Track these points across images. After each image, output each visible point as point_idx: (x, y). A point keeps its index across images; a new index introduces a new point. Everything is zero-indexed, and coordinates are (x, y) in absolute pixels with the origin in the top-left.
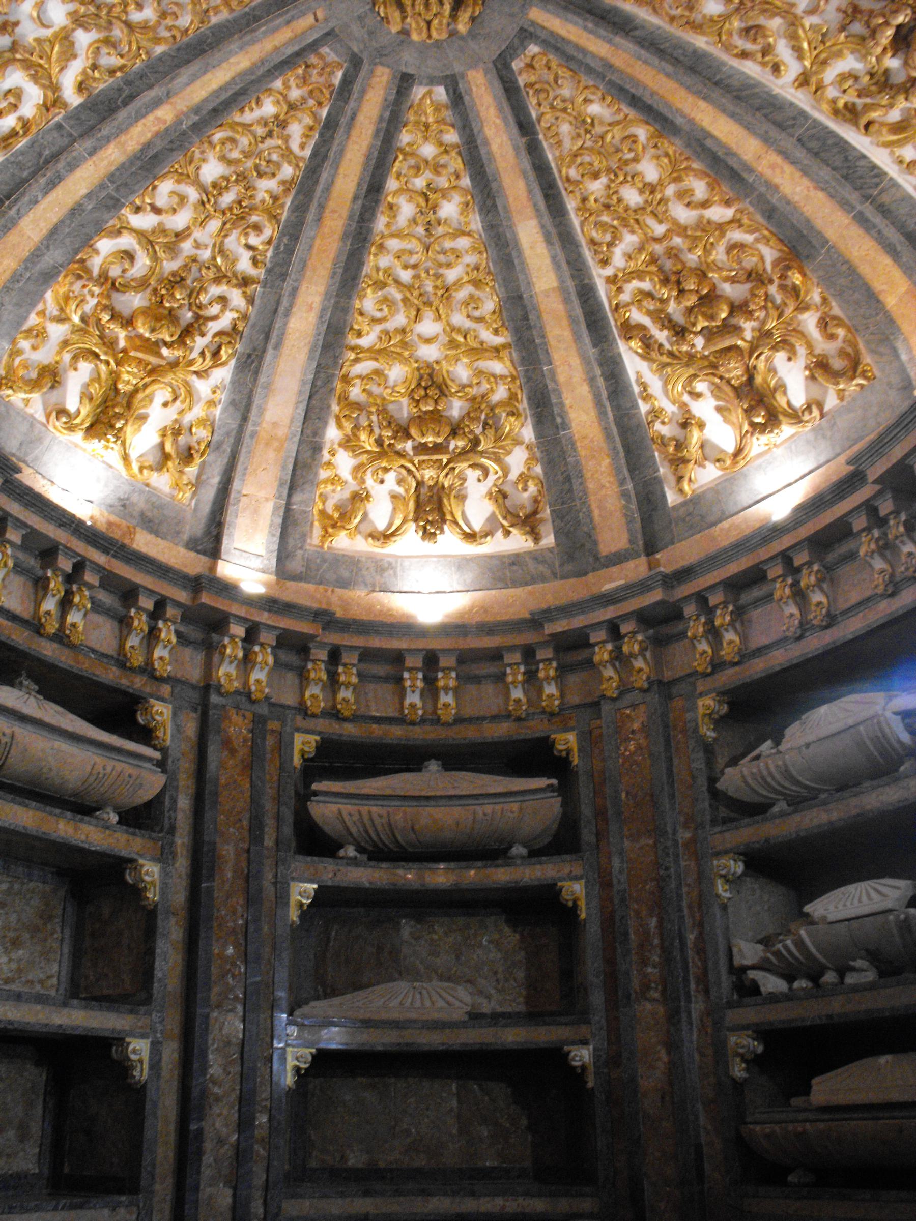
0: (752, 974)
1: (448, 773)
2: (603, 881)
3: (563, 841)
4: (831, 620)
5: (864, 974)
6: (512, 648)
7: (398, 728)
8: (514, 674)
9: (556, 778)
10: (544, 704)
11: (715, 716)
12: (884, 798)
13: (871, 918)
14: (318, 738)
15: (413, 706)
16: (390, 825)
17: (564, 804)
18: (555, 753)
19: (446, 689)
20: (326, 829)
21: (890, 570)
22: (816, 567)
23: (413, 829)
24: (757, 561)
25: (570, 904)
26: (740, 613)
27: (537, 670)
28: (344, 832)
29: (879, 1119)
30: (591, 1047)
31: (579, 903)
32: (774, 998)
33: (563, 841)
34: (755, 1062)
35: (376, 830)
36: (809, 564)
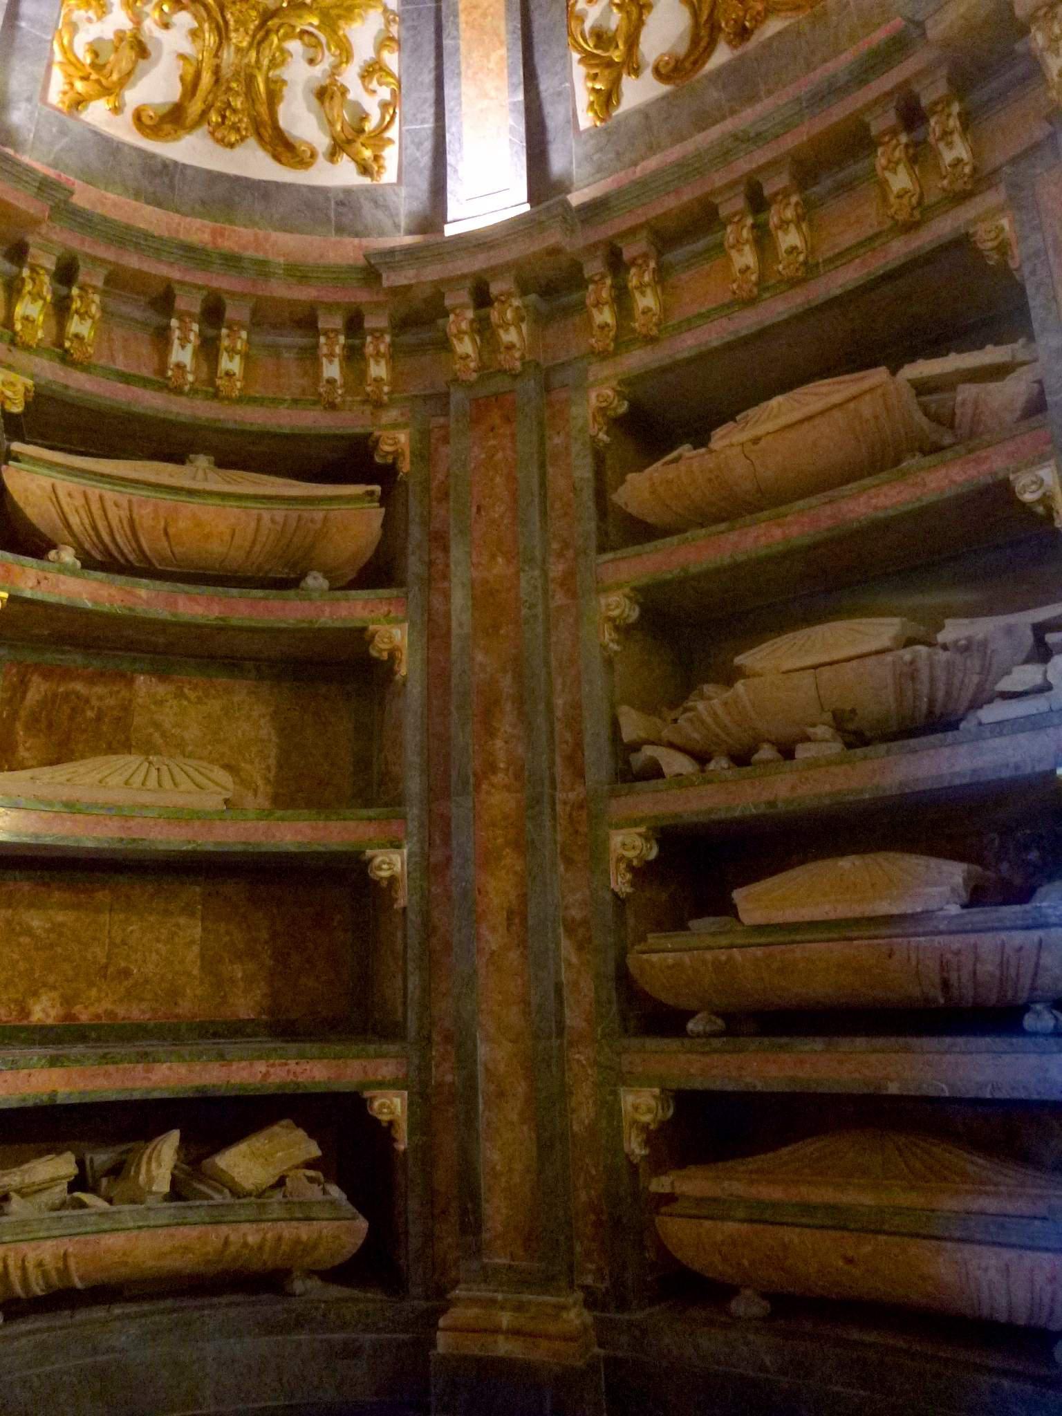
0: (648, 751)
1: (223, 472)
2: (435, 632)
3: (378, 572)
4: (810, 270)
5: (824, 745)
6: (331, 307)
7: (157, 395)
8: (331, 345)
9: (378, 483)
10: (369, 389)
11: (611, 413)
12: (881, 501)
13: (854, 663)
14: (30, 383)
15: (180, 366)
16: (131, 521)
17: (386, 524)
18: (378, 460)
19: (232, 351)
20: (30, 512)
21: (918, 189)
22: (794, 199)
23: (166, 533)
24: (707, 189)
25: (385, 656)
26: (662, 274)
27: (363, 345)
28: (60, 524)
29: (851, 939)
30: (405, 851)
31: (398, 654)
32: (680, 781)
33: (378, 572)
34: (642, 873)
35: (110, 526)
36: (786, 193)
